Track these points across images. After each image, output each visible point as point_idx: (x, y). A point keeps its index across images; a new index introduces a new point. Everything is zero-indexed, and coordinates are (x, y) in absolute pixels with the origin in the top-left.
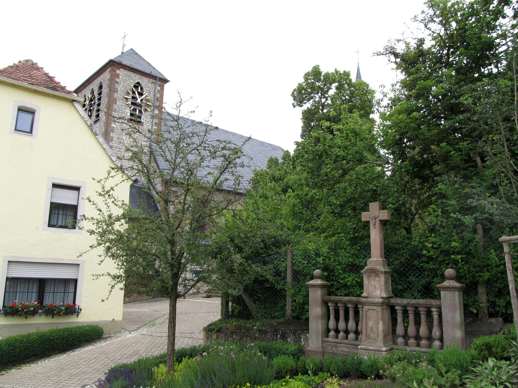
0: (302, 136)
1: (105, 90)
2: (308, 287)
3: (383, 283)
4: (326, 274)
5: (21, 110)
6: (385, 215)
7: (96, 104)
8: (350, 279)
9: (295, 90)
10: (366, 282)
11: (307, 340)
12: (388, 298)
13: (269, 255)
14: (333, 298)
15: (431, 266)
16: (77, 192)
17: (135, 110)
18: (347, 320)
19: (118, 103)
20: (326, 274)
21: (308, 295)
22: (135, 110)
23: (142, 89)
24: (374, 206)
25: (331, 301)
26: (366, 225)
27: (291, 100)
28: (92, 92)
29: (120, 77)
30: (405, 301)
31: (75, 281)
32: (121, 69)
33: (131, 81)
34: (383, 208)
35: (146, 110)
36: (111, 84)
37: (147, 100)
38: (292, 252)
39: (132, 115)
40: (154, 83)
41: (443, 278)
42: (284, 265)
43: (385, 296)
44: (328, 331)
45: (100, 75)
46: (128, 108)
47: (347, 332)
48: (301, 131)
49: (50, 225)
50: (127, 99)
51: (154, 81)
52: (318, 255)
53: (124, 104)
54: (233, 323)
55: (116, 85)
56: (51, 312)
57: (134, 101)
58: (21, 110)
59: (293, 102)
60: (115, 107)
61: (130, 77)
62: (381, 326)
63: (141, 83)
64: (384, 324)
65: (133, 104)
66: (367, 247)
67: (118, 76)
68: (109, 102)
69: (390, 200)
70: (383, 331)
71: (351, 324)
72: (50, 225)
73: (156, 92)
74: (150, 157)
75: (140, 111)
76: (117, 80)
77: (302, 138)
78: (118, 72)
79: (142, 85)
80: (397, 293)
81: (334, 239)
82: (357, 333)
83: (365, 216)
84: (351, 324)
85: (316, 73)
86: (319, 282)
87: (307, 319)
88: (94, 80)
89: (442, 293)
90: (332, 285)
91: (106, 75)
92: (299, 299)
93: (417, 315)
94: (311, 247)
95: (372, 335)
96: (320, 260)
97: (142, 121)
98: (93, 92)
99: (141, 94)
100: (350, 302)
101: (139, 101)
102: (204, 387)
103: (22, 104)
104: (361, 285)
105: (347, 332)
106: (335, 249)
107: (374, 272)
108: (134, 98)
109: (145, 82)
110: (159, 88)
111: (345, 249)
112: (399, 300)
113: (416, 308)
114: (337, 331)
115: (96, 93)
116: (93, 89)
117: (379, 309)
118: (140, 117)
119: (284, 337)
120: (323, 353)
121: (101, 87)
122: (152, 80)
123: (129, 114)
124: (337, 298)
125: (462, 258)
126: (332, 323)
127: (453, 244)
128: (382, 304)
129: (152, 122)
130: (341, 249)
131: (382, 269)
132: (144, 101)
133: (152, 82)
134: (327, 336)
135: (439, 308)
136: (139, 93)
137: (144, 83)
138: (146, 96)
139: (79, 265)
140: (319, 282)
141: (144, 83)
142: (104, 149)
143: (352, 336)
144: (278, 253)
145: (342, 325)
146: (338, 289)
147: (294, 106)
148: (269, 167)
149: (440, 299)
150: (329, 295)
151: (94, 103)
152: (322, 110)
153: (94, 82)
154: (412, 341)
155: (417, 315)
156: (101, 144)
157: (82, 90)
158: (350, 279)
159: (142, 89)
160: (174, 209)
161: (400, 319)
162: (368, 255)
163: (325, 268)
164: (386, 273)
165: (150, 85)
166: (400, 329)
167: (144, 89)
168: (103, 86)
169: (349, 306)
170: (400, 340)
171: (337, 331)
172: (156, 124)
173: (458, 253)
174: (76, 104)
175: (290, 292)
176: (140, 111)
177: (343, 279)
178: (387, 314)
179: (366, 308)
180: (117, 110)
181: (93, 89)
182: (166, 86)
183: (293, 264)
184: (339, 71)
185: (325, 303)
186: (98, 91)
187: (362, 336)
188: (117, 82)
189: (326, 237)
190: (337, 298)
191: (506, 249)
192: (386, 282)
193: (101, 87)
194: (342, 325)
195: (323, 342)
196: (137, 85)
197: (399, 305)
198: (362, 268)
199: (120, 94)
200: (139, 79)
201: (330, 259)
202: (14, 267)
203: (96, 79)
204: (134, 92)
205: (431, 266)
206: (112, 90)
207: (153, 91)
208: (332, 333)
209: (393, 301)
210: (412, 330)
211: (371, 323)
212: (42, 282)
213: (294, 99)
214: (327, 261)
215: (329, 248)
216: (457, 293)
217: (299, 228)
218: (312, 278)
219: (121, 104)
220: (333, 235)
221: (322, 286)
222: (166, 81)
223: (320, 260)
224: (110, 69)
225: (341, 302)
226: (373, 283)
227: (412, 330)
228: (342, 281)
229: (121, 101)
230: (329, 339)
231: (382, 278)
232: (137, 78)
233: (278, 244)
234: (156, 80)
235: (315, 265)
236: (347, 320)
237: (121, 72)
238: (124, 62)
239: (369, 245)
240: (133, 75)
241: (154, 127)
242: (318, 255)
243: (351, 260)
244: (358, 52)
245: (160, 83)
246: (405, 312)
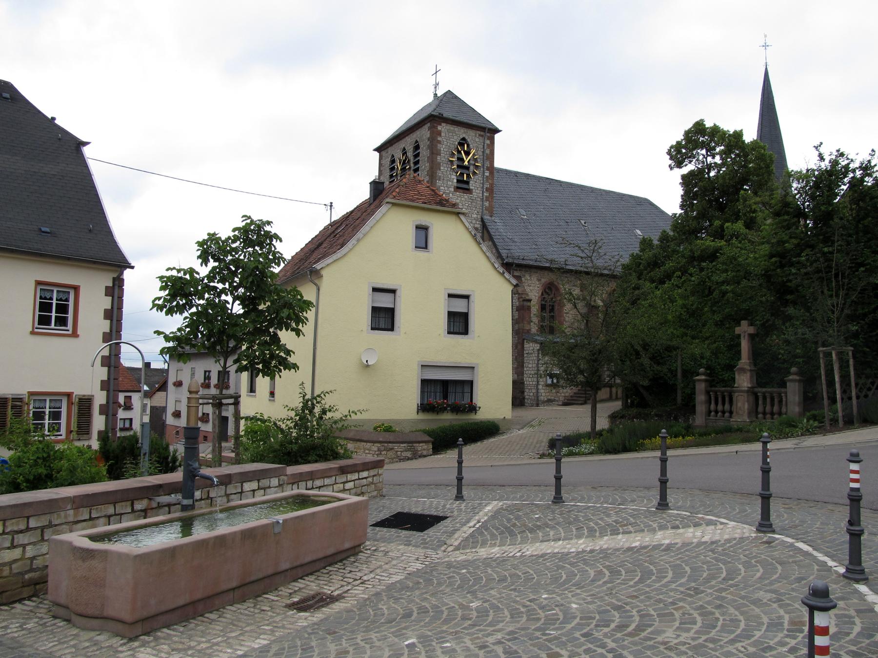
0: (682, 207)
1: (424, 152)
2: (694, 381)
3: (748, 377)
4: (708, 372)
5: (418, 227)
6: (751, 330)
7: (412, 169)
8: (726, 376)
9: (672, 147)
10: (737, 376)
11: (694, 420)
12: (752, 387)
13: (662, 358)
14: (713, 389)
15: (785, 365)
16: (467, 300)
17: (462, 174)
18: (724, 404)
19: (442, 168)
20: (708, 372)
21: (695, 388)
22: (462, 174)
23: (468, 146)
24: (744, 323)
25: (712, 391)
26: (739, 336)
27: (667, 161)
28: (404, 153)
29: (443, 134)
30: (764, 390)
31: (471, 383)
32: (443, 124)
33: (455, 137)
34: (751, 324)
35: (474, 173)
36: (432, 145)
37: (476, 160)
38: (681, 355)
39: (458, 181)
40: (482, 136)
41: (789, 373)
42: (675, 365)
43: (750, 386)
44: (710, 412)
45: (414, 131)
46: (454, 174)
47: (723, 412)
48: (681, 200)
49: (449, 333)
50: (452, 162)
51: (482, 133)
52: (702, 358)
53: (449, 169)
54: (634, 411)
55: (439, 145)
56: (456, 409)
57: (460, 163)
58: (418, 227)
59: (670, 162)
60: (439, 174)
61: (454, 132)
62: (746, 406)
63: (467, 138)
64: (749, 404)
65: (458, 166)
66: (739, 352)
67: (439, 133)
68: (431, 168)
69: (757, 318)
70: (748, 409)
71: (727, 407)
72: (449, 333)
73: (486, 148)
74: (483, 233)
75: (468, 175)
76: (439, 139)
77: (682, 209)
78: (439, 128)
79: (468, 140)
80: (760, 384)
81: (715, 345)
82: (731, 412)
83: (738, 330)
84: (727, 407)
85: (699, 128)
86: (703, 377)
87: (694, 406)
88: (405, 137)
89: (788, 384)
90: (713, 380)
91: (424, 133)
92: (688, 391)
93: (772, 399)
94: (697, 351)
95: (740, 412)
96: (704, 361)
97: (471, 187)
98: (406, 153)
99: (467, 153)
100: (726, 391)
101: (466, 163)
102: (876, 198)
103: (418, 223)
104: (733, 379)
105: (723, 412)
106: (716, 353)
107: (743, 370)
108: (461, 159)
109: (472, 137)
110: (488, 142)
111: (724, 354)
112: (760, 389)
113: (771, 394)
114: (716, 412)
115: (410, 154)
116: (404, 149)
117: (746, 395)
118: (467, 183)
119: (676, 419)
120: (706, 426)
121: (417, 147)
122: (479, 132)
123: (455, 181)
124: (717, 389)
125: (803, 361)
126: (713, 407)
127: (798, 351)
128: (748, 392)
129: (483, 188)
130: (720, 353)
131: (748, 367)
132: (471, 162)
133: (480, 135)
134: (709, 416)
135: (786, 393)
136: (465, 152)
137: (470, 137)
138: (474, 155)
139: (473, 368)
140: (703, 377)
141: (470, 137)
142: (488, 257)
143: (727, 415)
144: (669, 356)
145: (720, 407)
146: (717, 383)
147: (671, 168)
148: (642, 250)
149: (786, 388)
150: (711, 386)
151: (410, 168)
152: (708, 173)
153: (405, 139)
154: (768, 416)
155: (772, 399)
156: (484, 253)
157: (388, 147)
158: (726, 376)
159: (468, 146)
160: (519, 299)
161: (760, 402)
162: (739, 359)
163: (708, 368)
164: (751, 370)
165: (477, 140)
166: (760, 409)
167: (471, 146)
168: (421, 146)
169: (725, 394)
170: (760, 416)
171: (716, 412)
172: (487, 189)
173: (799, 357)
174: (462, 217)
175: (680, 384)
176: (468, 175)
177: (722, 375)
178: (752, 399)
179: (736, 394)
180: (442, 178)
181: (404, 149)
182: (497, 136)
183: (683, 365)
184: (728, 131)
185: (708, 393)
186: (414, 152)
187: (734, 414)
188: (439, 142)
189: (709, 344)
190: (717, 389)
191: (821, 356)
192: (751, 377)
193: (417, 147)
194: (720, 407)
195: (706, 419)
196: (463, 142)
197: (760, 392)
198: (736, 366)
199: (443, 158)
200: (464, 133)
201: (712, 361)
202: (426, 370)
203: (408, 135)
204: (459, 152)
205: (785, 365)
206: (434, 151)
207: (482, 147)
208: (713, 413)
209: (756, 390)
210: (768, 408)
211: (739, 404)
212: (445, 384)
213: (671, 159)
214: (710, 363)
215: (711, 353)
216: (797, 384)
217: (686, 335)
218: (698, 375)
219: (446, 169)
220: (715, 342)
221: (705, 381)
222: (497, 131)
223: (704, 361)
224: (429, 125)
225: (720, 391)
226: (742, 377)
227: (768, 408)
228: (720, 377)
229: (445, 165)
230: (711, 418)
231: (748, 374)
232: (461, 133)
233: (669, 349)
234: (485, 132)
235: (701, 366)
236: (724, 404)
237: (443, 128)
238: (446, 114)
239: (740, 351)
240: (457, 129)
241: (485, 194)
242: (702, 358)
243: (728, 362)
244: (765, 46)
245: (488, 135)
246: (765, 398)
